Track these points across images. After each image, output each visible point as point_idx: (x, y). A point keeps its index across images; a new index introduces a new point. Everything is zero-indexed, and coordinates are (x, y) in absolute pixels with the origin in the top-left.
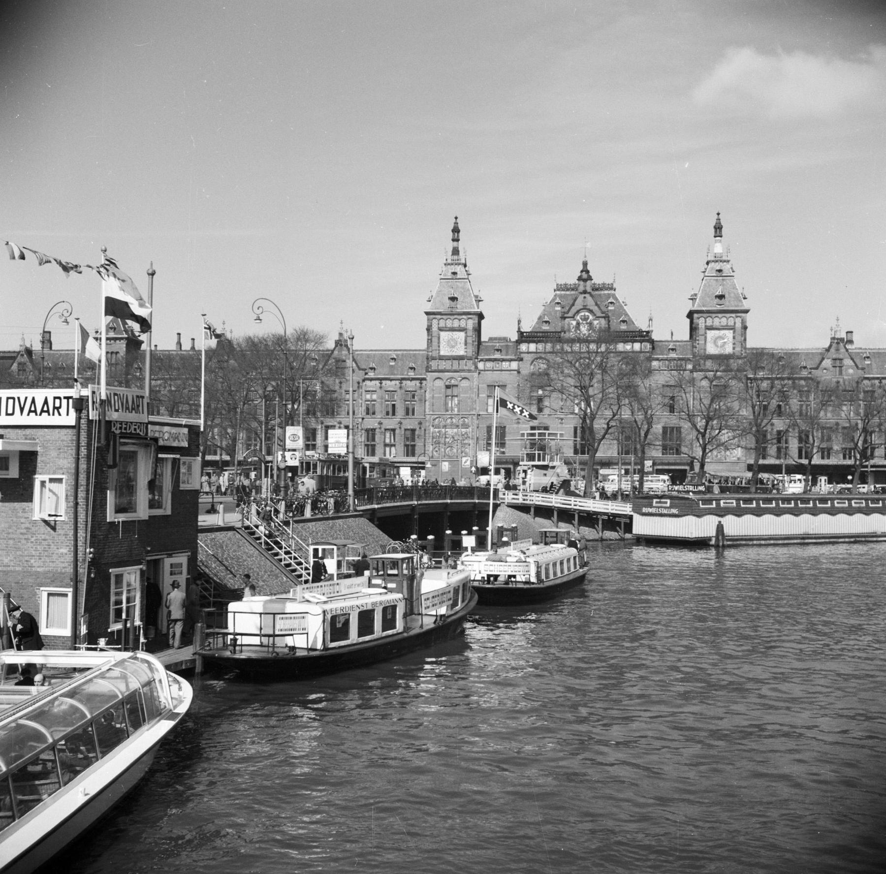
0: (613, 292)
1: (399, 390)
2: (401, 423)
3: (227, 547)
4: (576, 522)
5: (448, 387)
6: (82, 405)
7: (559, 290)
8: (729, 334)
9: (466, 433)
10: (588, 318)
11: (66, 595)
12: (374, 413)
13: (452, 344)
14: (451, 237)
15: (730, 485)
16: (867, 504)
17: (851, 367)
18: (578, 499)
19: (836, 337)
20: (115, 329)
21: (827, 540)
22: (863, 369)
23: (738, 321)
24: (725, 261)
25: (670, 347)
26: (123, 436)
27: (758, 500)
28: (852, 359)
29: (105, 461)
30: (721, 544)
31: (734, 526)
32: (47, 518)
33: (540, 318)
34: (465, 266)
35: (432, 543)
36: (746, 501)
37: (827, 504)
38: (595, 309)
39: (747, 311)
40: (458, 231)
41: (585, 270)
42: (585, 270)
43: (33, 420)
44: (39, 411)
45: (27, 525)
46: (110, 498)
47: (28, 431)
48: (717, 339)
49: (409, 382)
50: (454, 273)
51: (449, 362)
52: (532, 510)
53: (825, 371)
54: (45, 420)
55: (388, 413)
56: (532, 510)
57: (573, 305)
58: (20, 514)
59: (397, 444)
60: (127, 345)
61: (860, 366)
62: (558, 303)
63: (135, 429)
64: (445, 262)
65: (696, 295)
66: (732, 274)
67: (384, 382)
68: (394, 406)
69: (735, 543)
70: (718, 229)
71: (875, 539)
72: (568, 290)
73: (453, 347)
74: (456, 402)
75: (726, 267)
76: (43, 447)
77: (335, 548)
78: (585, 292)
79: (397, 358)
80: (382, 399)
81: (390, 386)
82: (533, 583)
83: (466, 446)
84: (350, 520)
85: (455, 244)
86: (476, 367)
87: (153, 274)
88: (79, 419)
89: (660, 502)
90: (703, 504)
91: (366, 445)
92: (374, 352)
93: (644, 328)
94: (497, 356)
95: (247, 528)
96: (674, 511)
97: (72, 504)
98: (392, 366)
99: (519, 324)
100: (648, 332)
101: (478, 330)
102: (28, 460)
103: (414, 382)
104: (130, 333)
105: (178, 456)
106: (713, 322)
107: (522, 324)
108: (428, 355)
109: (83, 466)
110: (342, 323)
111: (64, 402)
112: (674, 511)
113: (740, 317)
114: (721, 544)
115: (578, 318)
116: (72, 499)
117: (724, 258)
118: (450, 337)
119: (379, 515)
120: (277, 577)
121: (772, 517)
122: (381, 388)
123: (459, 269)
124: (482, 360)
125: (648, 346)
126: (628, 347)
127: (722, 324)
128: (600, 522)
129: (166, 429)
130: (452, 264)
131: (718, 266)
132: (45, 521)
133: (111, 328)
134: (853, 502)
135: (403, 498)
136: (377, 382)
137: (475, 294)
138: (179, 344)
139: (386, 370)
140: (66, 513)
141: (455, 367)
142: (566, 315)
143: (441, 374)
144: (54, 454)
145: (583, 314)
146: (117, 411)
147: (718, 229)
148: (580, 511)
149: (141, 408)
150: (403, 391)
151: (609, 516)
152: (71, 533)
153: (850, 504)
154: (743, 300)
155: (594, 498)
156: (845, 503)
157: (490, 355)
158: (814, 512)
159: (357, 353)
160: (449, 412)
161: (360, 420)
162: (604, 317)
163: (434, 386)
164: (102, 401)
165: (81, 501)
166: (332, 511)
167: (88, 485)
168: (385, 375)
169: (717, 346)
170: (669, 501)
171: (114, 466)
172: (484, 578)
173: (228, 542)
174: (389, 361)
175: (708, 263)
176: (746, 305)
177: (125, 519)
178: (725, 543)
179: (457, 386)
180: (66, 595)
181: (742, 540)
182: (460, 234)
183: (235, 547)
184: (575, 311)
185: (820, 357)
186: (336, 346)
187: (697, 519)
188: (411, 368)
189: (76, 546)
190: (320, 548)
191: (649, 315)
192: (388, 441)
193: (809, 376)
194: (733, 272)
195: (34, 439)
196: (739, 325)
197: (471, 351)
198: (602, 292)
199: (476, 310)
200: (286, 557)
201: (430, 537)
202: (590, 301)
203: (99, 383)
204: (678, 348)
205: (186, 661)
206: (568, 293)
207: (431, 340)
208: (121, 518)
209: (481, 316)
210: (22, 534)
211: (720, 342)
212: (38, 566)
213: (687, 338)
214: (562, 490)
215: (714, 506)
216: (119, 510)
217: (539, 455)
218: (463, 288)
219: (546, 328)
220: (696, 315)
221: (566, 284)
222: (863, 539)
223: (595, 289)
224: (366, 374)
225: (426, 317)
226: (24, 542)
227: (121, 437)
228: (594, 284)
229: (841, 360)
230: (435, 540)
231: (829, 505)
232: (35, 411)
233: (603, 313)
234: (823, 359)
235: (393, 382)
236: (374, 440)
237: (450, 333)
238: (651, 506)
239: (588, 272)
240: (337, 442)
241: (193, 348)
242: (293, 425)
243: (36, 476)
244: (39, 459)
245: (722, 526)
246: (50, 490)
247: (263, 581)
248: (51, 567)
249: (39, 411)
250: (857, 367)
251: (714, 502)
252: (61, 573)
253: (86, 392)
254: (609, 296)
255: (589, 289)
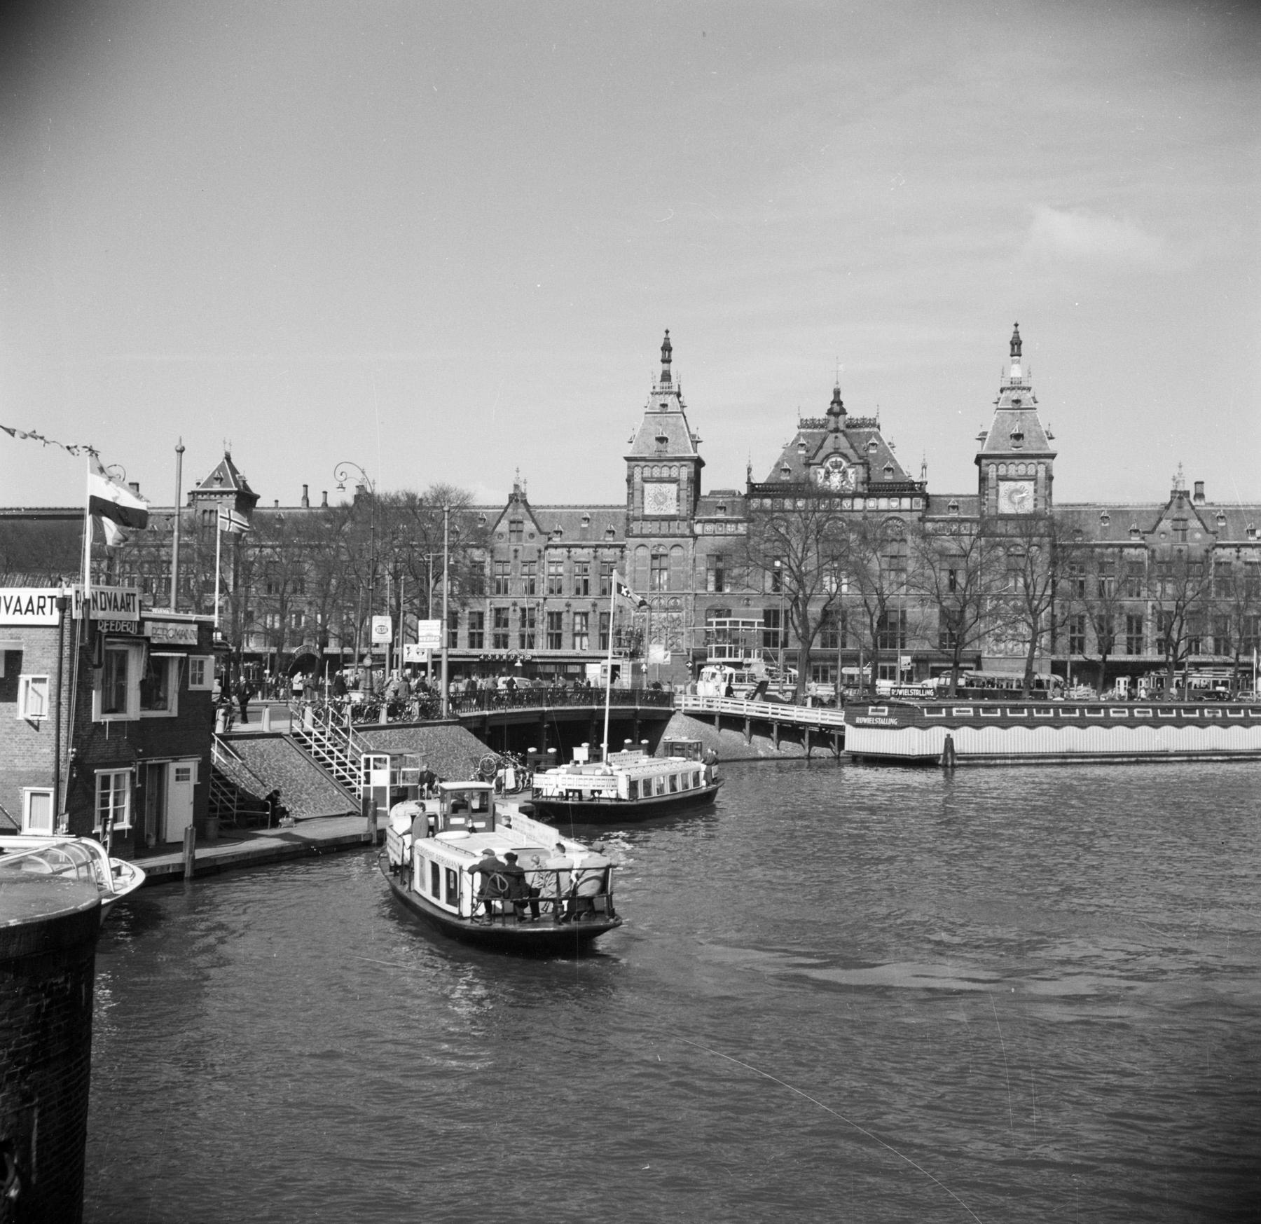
0: (876, 430)
1: (593, 561)
2: (568, 605)
3: (268, 755)
4: (774, 734)
5: (654, 557)
6: (65, 604)
7: (803, 427)
8: (1029, 486)
9: (678, 618)
10: (841, 466)
11: (48, 795)
12: (560, 591)
13: (660, 500)
14: (660, 358)
15: (995, 688)
16: (1155, 713)
17: (1198, 530)
18: (780, 706)
19: (1179, 489)
20: (221, 479)
21: (1098, 760)
22: (1214, 533)
23: (1042, 468)
24: (1024, 389)
25: (950, 504)
26: (109, 635)
27: (1030, 708)
28: (1199, 519)
29: (90, 660)
30: (950, 763)
31: (968, 740)
32: (31, 718)
33: (777, 465)
34: (679, 395)
35: (553, 757)
36: (987, 709)
37: (1023, 713)
38: (850, 452)
39: (1053, 456)
40: (670, 350)
41: (837, 401)
42: (837, 401)
43: (19, 619)
44: (24, 610)
45: (12, 725)
46: (96, 698)
47: (14, 630)
48: (1012, 493)
49: (606, 550)
50: (664, 406)
51: (656, 524)
52: (717, 719)
53: (1163, 536)
54: (29, 619)
55: (578, 592)
56: (717, 719)
57: (821, 447)
58: (5, 714)
59: (590, 632)
60: (237, 500)
61: (1211, 530)
62: (802, 445)
63: (125, 628)
64: (652, 390)
65: (985, 434)
66: (1034, 405)
67: (573, 550)
68: (586, 581)
69: (970, 762)
70: (1016, 344)
71: (1164, 759)
72: (815, 427)
73: (662, 503)
74: (666, 578)
75: (1026, 397)
76: (28, 646)
77: (388, 757)
78: (837, 430)
79: (590, 517)
80: (570, 572)
81: (580, 556)
82: (625, 800)
83: (679, 636)
84: (440, 728)
85: (666, 365)
86: (692, 531)
87: (181, 451)
88: (62, 618)
89: (876, 710)
90: (1011, 713)
91: (549, 634)
92: (560, 510)
93: (916, 479)
94: (720, 516)
95: (297, 735)
96: (893, 721)
97: (55, 704)
98: (584, 528)
99: (749, 473)
100: (921, 484)
101: (696, 481)
102: (14, 659)
103: (612, 551)
104: (241, 483)
105: (184, 655)
106: (1007, 471)
107: (753, 473)
108: (628, 515)
109: (66, 666)
110: (518, 471)
111: (48, 601)
112: (893, 721)
113: (1044, 463)
114: (950, 763)
115: (828, 465)
116: (54, 698)
117: (1024, 384)
118: (657, 490)
119: (492, 723)
120: (326, 790)
121: (1075, 729)
122: (569, 557)
123: (671, 400)
124: (699, 521)
125: (920, 503)
126: (894, 504)
127: (1020, 473)
128: (807, 735)
129: (171, 625)
130: (661, 393)
131: (1015, 395)
132: (30, 722)
133: (217, 479)
134: (1111, 711)
135: (530, 702)
136: (565, 550)
137: (692, 433)
138: (306, 498)
139: (576, 534)
140: (50, 713)
141: (664, 531)
142: (811, 461)
143: (646, 539)
144: (38, 653)
145: (833, 459)
146: (103, 609)
147: (1016, 344)
148: (781, 722)
149: (131, 607)
150: (599, 562)
151: (820, 728)
152: (54, 732)
153: (1131, 714)
154: (1049, 442)
155: (805, 705)
156: (1124, 712)
157: (709, 514)
158: (1082, 724)
159: (538, 511)
160: (657, 591)
161: (541, 601)
162: (862, 464)
163: (638, 555)
164: (87, 602)
165: (64, 701)
166: (416, 718)
167: (70, 685)
168: (574, 540)
169: (1014, 503)
170: (886, 709)
171: (99, 666)
172: (562, 793)
173: (272, 751)
174: (580, 523)
175: (1002, 391)
176: (1052, 447)
177: (112, 720)
178: (957, 762)
179: (666, 555)
180: (48, 795)
181: (979, 758)
182: (673, 353)
183: (279, 756)
184: (824, 455)
185: (1158, 516)
186: (510, 502)
187: (921, 731)
188: (609, 532)
189: (58, 746)
190: (372, 757)
191: (922, 461)
192: (578, 628)
193: (1143, 542)
194: (1036, 402)
195: (19, 638)
196: (1042, 475)
197: (685, 509)
198: (862, 430)
199: (693, 454)
200: (339, 768)
201: (552, 750)
202: (843, 443)
203: (83, 582)
204: (961, 506)
205: (174, 865)
206: (816, 431)
207: (632, 494)
208: (109, 718)
209: (699, 463)
210: (6, 733)
211: (1017, 498)
212: (21, 765)
213: (975, 491)
214: (759, 695)
215: (944, 715)
216: (106, 710)
217: (730, 649)
218: (675, 425)
219: (785, 477)
220: (984, 462)
221: (813, 420)
222: (1148, 759)
223: (851, 425)
224: (550, 539)
225: (626, 463)
226: (8, 741)
227: (106, 637)
228: (851, 419)
229: (1185, 520)
230: (557, 753)
231: (1174, 715)
232: (20, 610)
233: (860, 458)
234: (1160, 519)
235: (586, 550)
236: (559, 627)
237: (658, 485)
238: (866, 715)
239: (840, 403)
240: (429, 635)
241: (325, 504)
242: (379, 614)
243: (21, 676)
244: (24, 658)
245: (952, 740)
246: (33, 689)
247: (308, 794)
248: (33, 766)
249: (24, 610)
250: (1207, 530)
251: (944, 710)
252: (44, 773)
253: (69, 592)
254: (870, 435)
255: (842, 427)
